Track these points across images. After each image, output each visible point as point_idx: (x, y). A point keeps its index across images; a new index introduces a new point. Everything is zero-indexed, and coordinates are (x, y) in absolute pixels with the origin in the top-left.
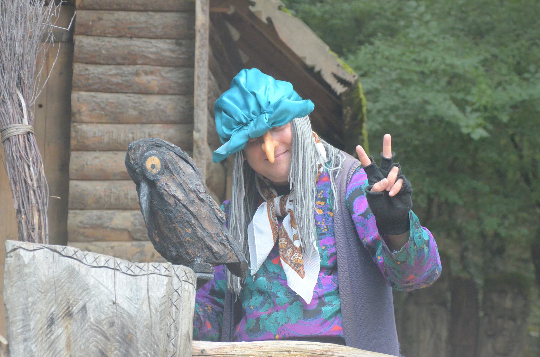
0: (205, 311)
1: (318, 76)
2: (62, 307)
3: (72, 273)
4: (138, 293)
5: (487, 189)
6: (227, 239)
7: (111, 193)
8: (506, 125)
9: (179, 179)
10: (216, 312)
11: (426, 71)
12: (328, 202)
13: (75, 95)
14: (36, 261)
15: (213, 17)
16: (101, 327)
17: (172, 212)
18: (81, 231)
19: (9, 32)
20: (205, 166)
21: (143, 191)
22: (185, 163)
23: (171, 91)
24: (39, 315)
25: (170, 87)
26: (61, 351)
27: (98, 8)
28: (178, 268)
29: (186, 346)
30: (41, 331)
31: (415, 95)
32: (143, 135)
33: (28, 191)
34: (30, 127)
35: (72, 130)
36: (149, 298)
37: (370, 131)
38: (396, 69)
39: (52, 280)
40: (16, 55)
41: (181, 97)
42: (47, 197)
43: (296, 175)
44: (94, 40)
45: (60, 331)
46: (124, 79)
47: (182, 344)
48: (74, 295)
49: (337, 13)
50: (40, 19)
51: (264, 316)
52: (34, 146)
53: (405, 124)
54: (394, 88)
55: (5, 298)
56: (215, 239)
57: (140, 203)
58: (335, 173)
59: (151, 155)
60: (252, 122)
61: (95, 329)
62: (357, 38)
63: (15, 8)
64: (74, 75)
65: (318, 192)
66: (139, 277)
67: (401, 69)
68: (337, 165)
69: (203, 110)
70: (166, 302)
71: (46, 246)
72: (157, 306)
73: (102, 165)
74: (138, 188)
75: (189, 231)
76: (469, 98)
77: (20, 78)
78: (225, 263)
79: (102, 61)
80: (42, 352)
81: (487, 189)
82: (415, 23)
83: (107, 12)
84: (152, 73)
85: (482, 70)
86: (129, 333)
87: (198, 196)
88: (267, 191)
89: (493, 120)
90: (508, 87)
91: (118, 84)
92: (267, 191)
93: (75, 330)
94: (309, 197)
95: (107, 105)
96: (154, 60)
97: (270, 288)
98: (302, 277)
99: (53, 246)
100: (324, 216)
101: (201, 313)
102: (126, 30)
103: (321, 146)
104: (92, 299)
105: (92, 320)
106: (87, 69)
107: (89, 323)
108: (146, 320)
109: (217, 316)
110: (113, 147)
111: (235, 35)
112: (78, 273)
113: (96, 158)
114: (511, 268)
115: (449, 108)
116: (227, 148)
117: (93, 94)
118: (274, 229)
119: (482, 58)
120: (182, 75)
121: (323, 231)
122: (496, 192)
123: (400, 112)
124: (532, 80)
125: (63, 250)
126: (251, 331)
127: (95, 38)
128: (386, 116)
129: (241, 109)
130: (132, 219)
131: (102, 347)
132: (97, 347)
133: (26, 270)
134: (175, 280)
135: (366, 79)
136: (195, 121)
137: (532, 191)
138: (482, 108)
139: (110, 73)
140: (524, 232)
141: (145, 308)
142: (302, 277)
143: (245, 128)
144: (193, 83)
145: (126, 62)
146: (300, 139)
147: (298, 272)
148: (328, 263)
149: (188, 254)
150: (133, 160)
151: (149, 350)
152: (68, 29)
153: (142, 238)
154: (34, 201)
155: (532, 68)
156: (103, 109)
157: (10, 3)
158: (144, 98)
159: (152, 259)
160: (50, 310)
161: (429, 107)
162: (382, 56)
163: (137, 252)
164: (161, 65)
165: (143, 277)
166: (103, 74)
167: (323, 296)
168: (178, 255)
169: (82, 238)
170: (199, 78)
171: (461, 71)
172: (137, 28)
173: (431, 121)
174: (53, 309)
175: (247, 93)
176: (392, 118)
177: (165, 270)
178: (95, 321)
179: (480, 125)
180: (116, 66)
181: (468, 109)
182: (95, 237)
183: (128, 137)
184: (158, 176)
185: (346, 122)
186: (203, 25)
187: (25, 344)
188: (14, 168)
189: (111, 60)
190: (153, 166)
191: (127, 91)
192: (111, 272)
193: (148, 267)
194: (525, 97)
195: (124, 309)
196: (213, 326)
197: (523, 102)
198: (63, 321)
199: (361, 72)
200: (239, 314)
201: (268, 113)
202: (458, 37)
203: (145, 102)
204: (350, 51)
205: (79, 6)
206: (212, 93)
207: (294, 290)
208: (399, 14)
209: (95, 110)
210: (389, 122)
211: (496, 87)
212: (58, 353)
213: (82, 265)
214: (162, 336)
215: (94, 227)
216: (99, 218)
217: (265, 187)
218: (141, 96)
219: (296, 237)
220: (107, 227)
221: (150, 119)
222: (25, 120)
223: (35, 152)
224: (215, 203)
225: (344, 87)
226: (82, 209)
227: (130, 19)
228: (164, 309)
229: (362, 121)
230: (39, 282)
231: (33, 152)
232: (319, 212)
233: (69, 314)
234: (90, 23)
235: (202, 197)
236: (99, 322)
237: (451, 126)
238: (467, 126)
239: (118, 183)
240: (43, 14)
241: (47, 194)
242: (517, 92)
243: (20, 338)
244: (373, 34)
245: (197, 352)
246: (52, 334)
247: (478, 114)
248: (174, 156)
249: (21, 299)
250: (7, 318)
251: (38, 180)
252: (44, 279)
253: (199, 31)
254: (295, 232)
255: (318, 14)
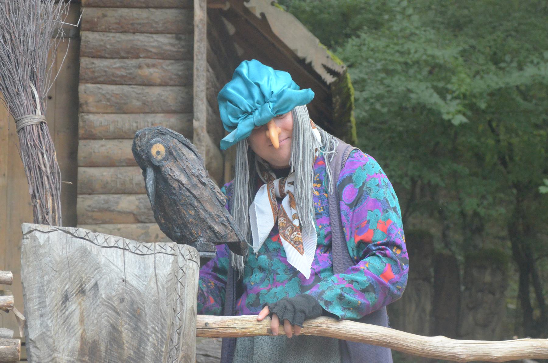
0: (208, 287)
1: (309, 67)
2: (76, 285)
3: (84, 253)
4: (146, 271)
5: (467, 171)
6: (228, 220)
7: (117, 178)
8: (484, 112)
9: (182, 164)
10: (218, 288)
11: (409, 61)
12: (324, 184)
13: (82, 87)
14: (50, 242)
15: (210, 12)
16: (112, 303)
17: (176, 195)
18: (90, 214)
19: (22, 28)
20: (204, 152)
21: (149, 176)
22: (187, 149)
23: (172, 83)
24: (54, 293)
25: (171, 79)
26: (75, 325)
27: (102, 5)
28: (182, 248)
29: (191, 320)
30: (56, 308)
31: (399, 84)
32: (146, 124)
33: (42, 177)
34: (43, 117)
35: (80, 120)
36: (156, 275)
37: (357, 118)
38: (381, 60)
39: (66, 259)
40: (29, 51)
41: (182, 88)
42: (59, 183)
43: (297, 159)
44: (100, 35)
45: (74, 307)
46: (127, 71)
47: (188, 318)
48: (86, 274)
49: (325, 8)
50: (51, 17)
51: (264, 291)
52: (47, 135)
53: (389, 112)
54: (379, 78)
55: (22, 276)
56: (217, 220)
57: (146, 188)
58: (330, 156)
59: (156, 142)
60: (257, 111)
61: (106, 305)
62: (344, 31)
63: (27, 6)
64: (80, 68)
65: (315, 174)
66: (147, 256)
67: (386, 60)
68: (331, 150)
69: (202, 100)
70: (172, 279)
71: (60, 228)
72: (164, 283)
73: (108, 152)
74: (145, 174)
75: (192, 212)
76: (449, 86)
77: (33, 72)
78: (226, 243)
79: (107, 55)
80: (58, 327)
81: (467, 171)
82: (399, 17)
83: (111, 9)
84: (154, 66)
85: (461, 60)
86: (138, 308)
87: (200, 180)
88: (266, 174)
89: (472, 107)
90: (485, 76)
91: (122, 77)
92: (266, 174)
93: (88, 306)
94: (308, 179)
95: (112, 96)
96: (155, 54)
97: (270, 265)
98: (302, 253)
99: (67, 228)
100: (320, 197)
101: (205, 289)
102: (129, 26)
103: (317, 132)
104: (103, 277)
105: (103, 296)
106: (93, 63)
107: (101, 299)
108: (153, 296)
109: (220, 291)
110: (119, 136)
111: (231, 29)
112: (90, 253)
113: (102, 146)
114: (489, 245)
115: (431, 96)
116: (234, 136)
117: (99, 86)
118: (274, 209)
119: (460, 48)
120: (182, 68)
121: (320, 211)
122: (475, 174)
123: (386, 100)
124: (508, 69)
125: (76, 232)
126: (252, 305)
127: (101, 33)
128: (372, 104)
129: (245, 99)
130: (137, 203)
131: (113, 322)
132: (109, 322)
133: (42, 251)
134: (180, 258)
135: (353, 70)
136: (195, 110)
137: (508, 173)
138: (461, 96)
139: (115, 66)
140: (501, 211)
141: (153, 285)
142: (302, 253)
143: (250, 116)
144: (192, 75)
145: (130, 55)
146: (300, 125)
147: (298, 249)
148: (325, 242)
149: (191, 234)
150: (140, 147)
151: (157, 324)
152: (77, 26)
153: (146, 221)
154: (47, 186)
155: (508, 58)
156: (108, 100)
157: (23, 2)
158: (147, 90)
159: (157, 239)
160: (64, 288)
161: (413, 96)
162: (368, 48)
163: (142, 234)
164: (163, 59)
165: (150, 256)
166: (108, 67)
167: (320, 272)
168: (182, 235)
169: (90, 221)
170: (198, 69)
171: (441, 62)
172: (140, 24)
173: (414, 109)
174: (67, 287)
175: (251, 83)
176: (378, 106)
177: (170, 249)
178: (106, 297)
179: (459, 112)
180: (120, 60)
181: (449, 97)
182: (102, 219)
183: (133, 126)
184: (163, 162)
185: (335, 110)
186: (201, 20)
187: (42, 319)
188: (28, 156)
189: (115, 54)
190: (158, 153)
191: (130, 83)
192: (120, 252)
193: (155, 247)
194: (501, 85)
195: (133, 286)
196: (215, 301)
197: (500, 89)
198: (76, 298)
199: (349, 63)
200: (241, 289)
201: (271, 102)
202: (438, 29)
203: (148, 93)
204: (337, 43)
205: (85, 4)
206: (210, 84)
207: (295, 266)
208: (383, 8)
209: (101, 101)
210: (374, 109)
211: (474, 76)
212: (72, 328)
213: (93, 245)
214: (169, 310)
215: (101, 210)
216: (107, 202)
217: (268, 171)
218: (144, 87)
219: (295, 217)
220: (113, 211)
221: (153, 109)
222: (39, 111)
223: (48, 141)
224: (216, 187)
225: (333, 77)
226: (90, 194)
227: (133, 16)
228: (171, 285)
229: (350, 109)
230: (54, 262)
231: (46, 140)
232: (317, 193)
233: (82, 291)
234: (96, 20)
235: (204, 181)
236: (110, 298)
237: (431, 112)
238: (448, 113)
239: (123, 169)
240: (53, 12)
241: (59, 180)
242: (494, 80)
243: (37, 314)
244: (359, 28)
245: (201, 325)
246: (67, 310)
247: (458, 101)
248: (178, 143)
249: (37, 278)
250: (24, 295)
251: (52, 167)
252: (58, 259)
253: (198, 26)
254: (294, 211)
255: (308, 9)
